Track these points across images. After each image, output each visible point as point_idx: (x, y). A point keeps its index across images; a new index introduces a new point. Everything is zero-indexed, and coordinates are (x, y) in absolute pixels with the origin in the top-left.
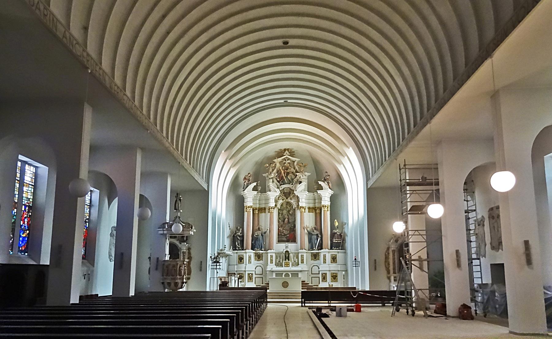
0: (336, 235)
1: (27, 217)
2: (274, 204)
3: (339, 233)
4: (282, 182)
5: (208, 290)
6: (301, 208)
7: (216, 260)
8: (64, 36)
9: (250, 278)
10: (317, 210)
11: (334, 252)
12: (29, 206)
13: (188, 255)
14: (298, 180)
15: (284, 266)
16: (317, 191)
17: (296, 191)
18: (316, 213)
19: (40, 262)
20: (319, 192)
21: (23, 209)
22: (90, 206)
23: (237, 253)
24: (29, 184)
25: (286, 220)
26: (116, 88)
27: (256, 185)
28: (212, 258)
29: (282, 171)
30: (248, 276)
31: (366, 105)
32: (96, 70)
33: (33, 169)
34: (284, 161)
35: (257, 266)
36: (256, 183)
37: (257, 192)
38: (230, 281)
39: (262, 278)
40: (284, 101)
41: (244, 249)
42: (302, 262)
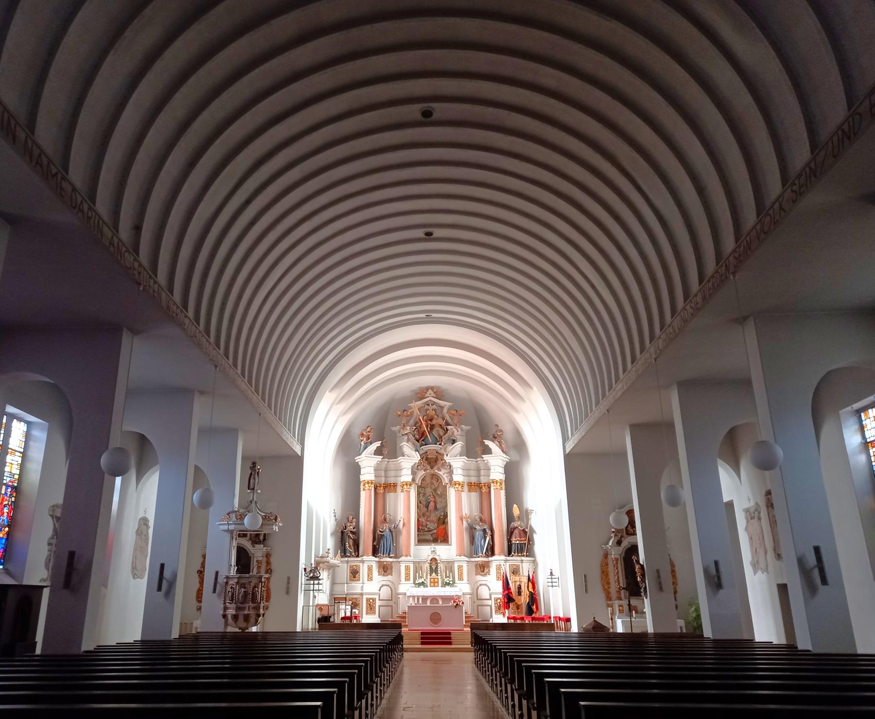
0: (516, 531)
1: (8, 504)
2: (411, 477)
3: (521, 527)
4: (423, 440)
5: (299, 629)
6: (455, 484)
7: (314, 575)
8: (111, 244)
9: (371, 608)
11: (515, 559)
12: (13, 487)
13: (267, 566)
14: (449, 439)
15: (429, 586)
16: (483, 456)
17: (447, 455)
18: (481, 493)
19: (22, 581)
20: (486, 457)
21: (3, 492)
24: (16, 451)
25: (432, 504)
26: (175, 307)
27: (380, 445)
28: (307, 570)
31: (557, 325)
32: (150, 286)
33: (22, 427)
34: (427, 407)
35: (383, 586)
36: (380, 442)
37: (382, 457)
38: (336, 612)
39: (392, 606)
40: (426, 316)
41: (360, 554)
42: (461, 578)
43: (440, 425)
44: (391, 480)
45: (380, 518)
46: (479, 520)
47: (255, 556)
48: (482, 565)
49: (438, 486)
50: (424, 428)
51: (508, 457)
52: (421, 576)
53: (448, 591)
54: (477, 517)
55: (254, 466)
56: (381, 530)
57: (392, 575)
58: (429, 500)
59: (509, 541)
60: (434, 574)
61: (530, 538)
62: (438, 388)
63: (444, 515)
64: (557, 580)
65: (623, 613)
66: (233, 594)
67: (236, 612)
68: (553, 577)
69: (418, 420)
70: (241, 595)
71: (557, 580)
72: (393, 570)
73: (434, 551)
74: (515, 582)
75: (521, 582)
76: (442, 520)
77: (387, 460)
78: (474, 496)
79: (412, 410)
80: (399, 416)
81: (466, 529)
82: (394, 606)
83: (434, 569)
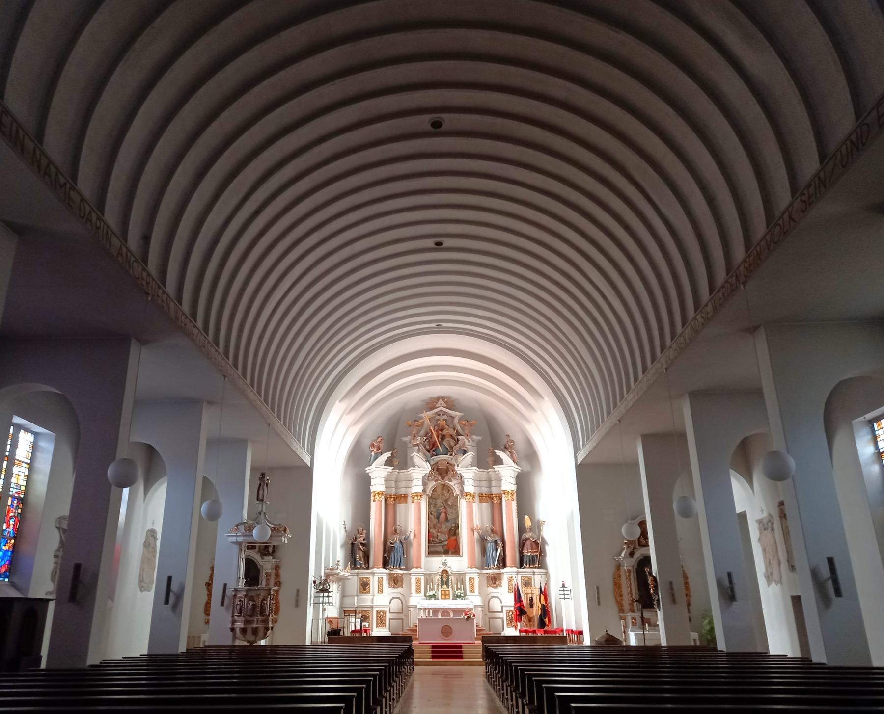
0: (528, 543)
1: (14, 516)
3: (533, 539)
4: (434, 451)
11: (527, 571)
12: (19, 499)
16: (494, 467)
17: (458, 466)
18: (492, 504)
25: (443, 515)
30: (377, 616)
34: (438, 417)
35: (393, 598)
36: (391, 453)
42: (472, 591)
43: (451, 435)
44: (402, 491)
45: (391, 530)
46: (490, 531)
50: (434, 438)
52: (432, 588)
53: (459, 604)
54: (488, 528)
55: (263, 477)
58: (440, 512)
59: (521, 553)
60: (445, 586)
63: (455, 526)
66: (241, 607)
68: (565, 589)
69: (428, 431)
70: (249, 608)
71: (569, 592)
73: (445, 563)
74: (527, 594)
75: (532, 594)
77: (397, 471)
78: (486, 506)
81: (478, 540)
82: (404, 618)
83: (445, 581)
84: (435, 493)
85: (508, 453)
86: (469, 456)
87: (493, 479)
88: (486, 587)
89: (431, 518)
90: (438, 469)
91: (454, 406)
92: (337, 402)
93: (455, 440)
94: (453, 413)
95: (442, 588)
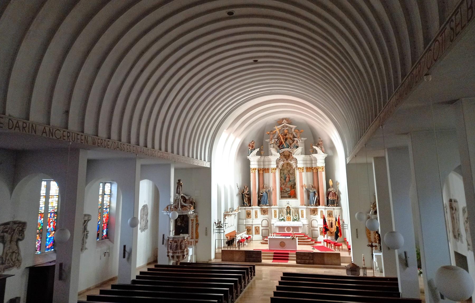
0: (331, 193)
1: (53, 221)
3: (334, 191)
4: (282, 146)
10: (312, 170)
11: (330, 208)
12: (55, 213)
16: (312, 154)
17: (294, 154)
18: (313, 173)
20: (314, 155)
22: (110, 195)
23: (245, 209)
24: (54, 196)
25: (287, 178)
29: (281, 137)
30: (255, 229)
34: (283, 128)
35: (263, 220)
36: (259, 149)
39: (268, 230)
41: (252, 205)
42: (302, 216)
43: (290, 138)
44: (267, 167)
45: (261, 186)
46: (311, 187)
47: (191, 217)
48: (314, 210)
49: (291, 169)
51: (326, 154)
52: (282, 215)
53: (295, 224)
54: (310, 185)
55: (179, 182)
56: (261, 192)
57: (268, 215)
58: (286, 177)
59: (327, 198)
61: (338, 196)
62: (289, 118)
63: (294, 184)
64: (346, 226)
65: (377, 250)
66: (171, 246)
67: (173, 254)
69: (278, 136)
70: (174, 246)
71: (346, 226)
72: (268, 212)
73: (288, 203)
74: (329, 220)
75: (332, 221)
76: (293, 187)
77: (263, 157)
78: (310, 174)
79: (276, 131)
80: (269, 134)
81: (305, 191)
82: (269, 229)
84: (283, 167)
85: (319, 147)
86: (300, 150)
87: (313, 160)
88: (310, 215)
89: (282, 180)
90: (284, 155)
91: (291, 122)
92: (225, 130)
93: (293, 140)
94: (291, 126)
95: (287, 215)
